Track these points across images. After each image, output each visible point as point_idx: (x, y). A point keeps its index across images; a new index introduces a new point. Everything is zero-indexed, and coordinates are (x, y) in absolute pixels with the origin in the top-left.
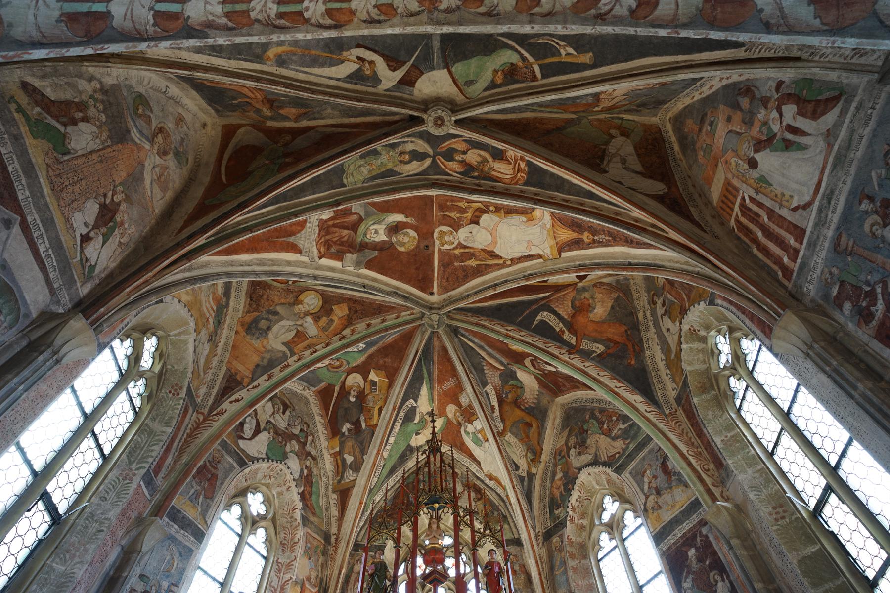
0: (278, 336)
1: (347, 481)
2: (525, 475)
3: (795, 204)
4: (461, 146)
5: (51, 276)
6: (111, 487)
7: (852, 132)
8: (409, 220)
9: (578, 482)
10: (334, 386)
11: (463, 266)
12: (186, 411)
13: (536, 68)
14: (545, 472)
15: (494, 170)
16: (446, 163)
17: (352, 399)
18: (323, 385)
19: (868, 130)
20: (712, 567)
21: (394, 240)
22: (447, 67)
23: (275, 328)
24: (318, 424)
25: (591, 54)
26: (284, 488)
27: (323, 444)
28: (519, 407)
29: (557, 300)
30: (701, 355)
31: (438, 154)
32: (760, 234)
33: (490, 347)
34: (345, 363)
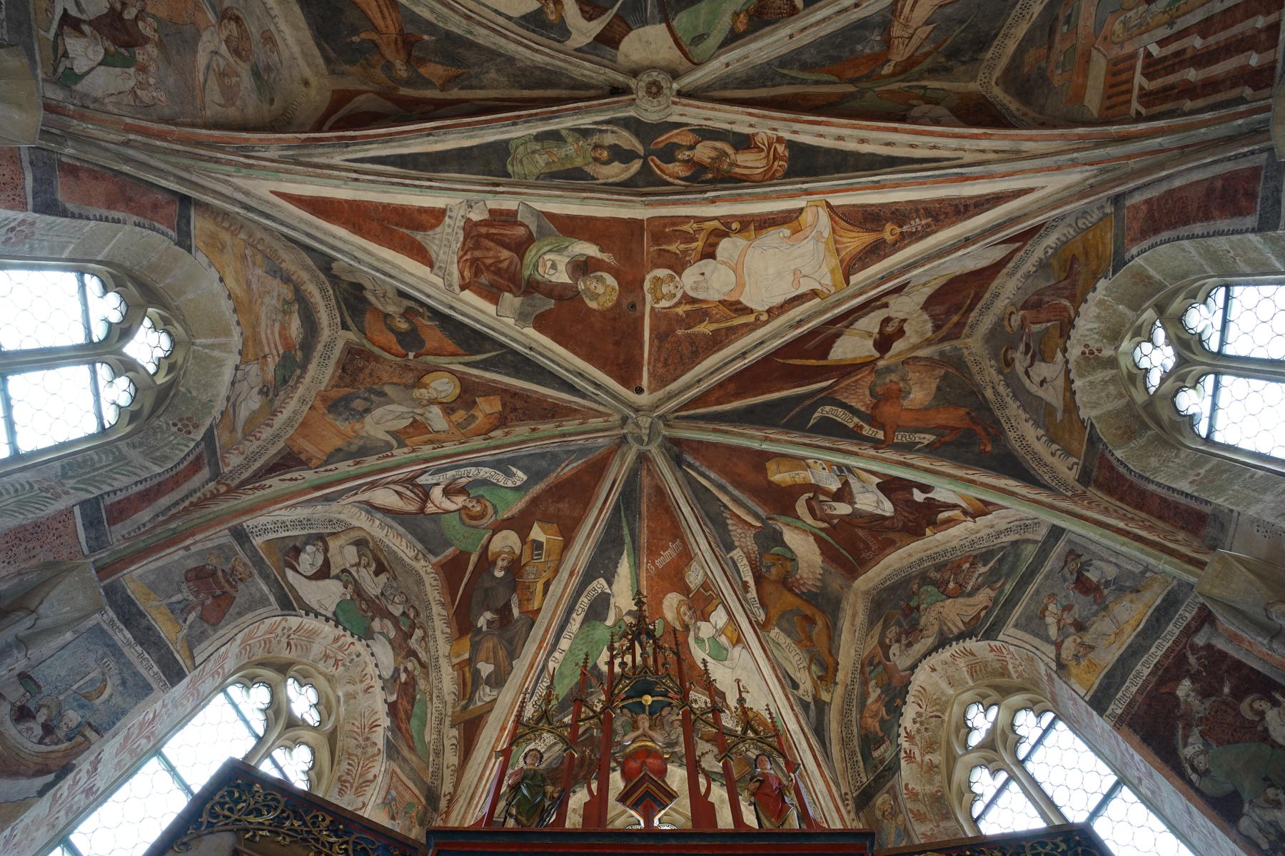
0: (381, 422)
1: (479, 704)
2: (810, 699)
4: (685, 139)
6: (12, 490)
8: (606, 257)
9: (913, 689)
10: (470, 554)
11: (690, 334)
12: (195, 466)
14: (847, 701)
15: (738, 166)
16: (664, 166)
17: (499, 574)
18: (450, 551)
20: (1238, 695)
21: (581, 286)
22: (666, 20)
23: (378, 413)
24: (436, 618)
26: (360, 687)
27: (440, 643)
28: (791, 590)
29: (846, 388)
30: (1111, 388)
32: (1192, 74)
33: (738, 485)
34: (490, 510)
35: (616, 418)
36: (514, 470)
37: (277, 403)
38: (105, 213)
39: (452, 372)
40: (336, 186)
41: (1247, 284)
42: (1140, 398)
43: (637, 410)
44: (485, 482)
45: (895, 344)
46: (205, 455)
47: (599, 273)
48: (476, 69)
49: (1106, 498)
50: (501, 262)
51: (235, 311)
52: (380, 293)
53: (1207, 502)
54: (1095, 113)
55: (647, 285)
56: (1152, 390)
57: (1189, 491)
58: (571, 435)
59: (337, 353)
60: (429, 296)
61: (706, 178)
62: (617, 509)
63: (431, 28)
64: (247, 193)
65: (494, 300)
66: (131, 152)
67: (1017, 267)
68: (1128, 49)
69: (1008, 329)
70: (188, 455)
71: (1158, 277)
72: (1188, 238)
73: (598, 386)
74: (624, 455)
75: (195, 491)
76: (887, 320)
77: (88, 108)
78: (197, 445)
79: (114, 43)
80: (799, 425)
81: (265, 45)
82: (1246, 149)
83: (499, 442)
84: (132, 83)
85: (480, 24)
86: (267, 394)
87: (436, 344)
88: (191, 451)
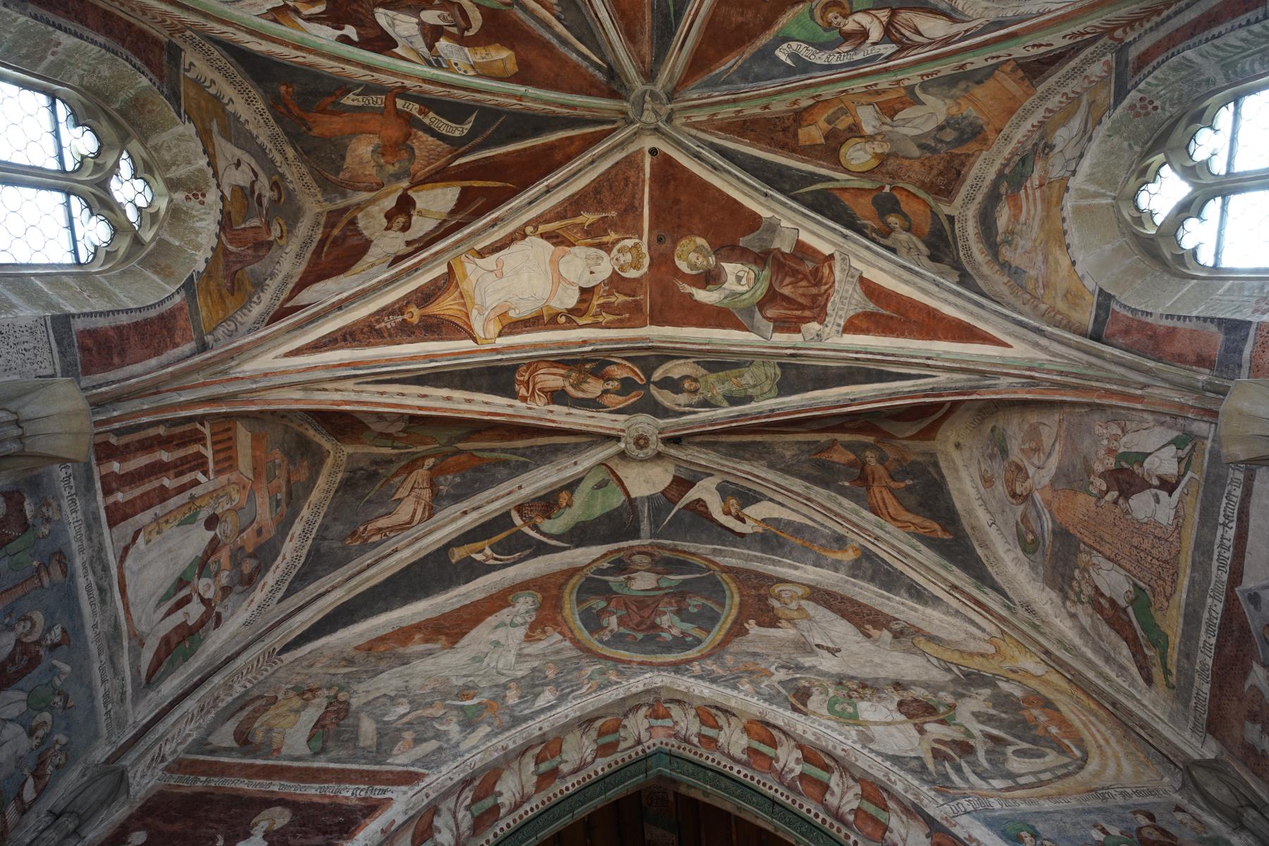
0: (929, 114)
3: (141, 540)
4: (611, 399)
5: (1238, 492)
7: (117, 672)
12: (1143, 60)
13: (518, 520)
16: (631, 375)
19: (101, 692)
21: (712, 260)
22: (631, 501)
23: (931, 126)
25: (453, 561)
29: (439, 156)
30: (167, 157)
32: (165, 456)
33: (547, 45)
34: (818, 13)
35: (678, 121)
36: (789, 62)
37: (1036, 136)
38: (1179, 324)
39: (847, 171)
40: (948, 353)
41: (60, 265)
42: (135, 145)
43: (657, 130)
44: (822, 47)
45: (394, 204)
47: (694, 272)
49: (145, 27)
50: (791, 283)
51: (1065, 233)
52: (914, 252)
53: (35, 17)
54: (239, 425)
55: (646, 261)
56: (125, 155)
57: (59, 33)
58: (727, 102)
59: (963, 192)
60: (868, 248)
61: (590, 364)
62: (679, 15)
63: (842, 491)
64: (1036, 345)
65: (800, 245)
66: (1142, 379)
67: (285, 283)
68: (223, 479)
69: (282, 222)
70: (1150, 73)
71: (148, 273)
72: (131, 310)
73: (698, 156)
74: (670, 80)
75: (1151, 29)
76: (405, 228)
77: (1169, 415)
78: (1137, 84)
79: (1133, 472)
80: (488, 114)
82: (103, 389)
83: (805, 92)
84: (1124, 439)
85: (799, 495)
86: (1046, 145)
87: (862, 200)
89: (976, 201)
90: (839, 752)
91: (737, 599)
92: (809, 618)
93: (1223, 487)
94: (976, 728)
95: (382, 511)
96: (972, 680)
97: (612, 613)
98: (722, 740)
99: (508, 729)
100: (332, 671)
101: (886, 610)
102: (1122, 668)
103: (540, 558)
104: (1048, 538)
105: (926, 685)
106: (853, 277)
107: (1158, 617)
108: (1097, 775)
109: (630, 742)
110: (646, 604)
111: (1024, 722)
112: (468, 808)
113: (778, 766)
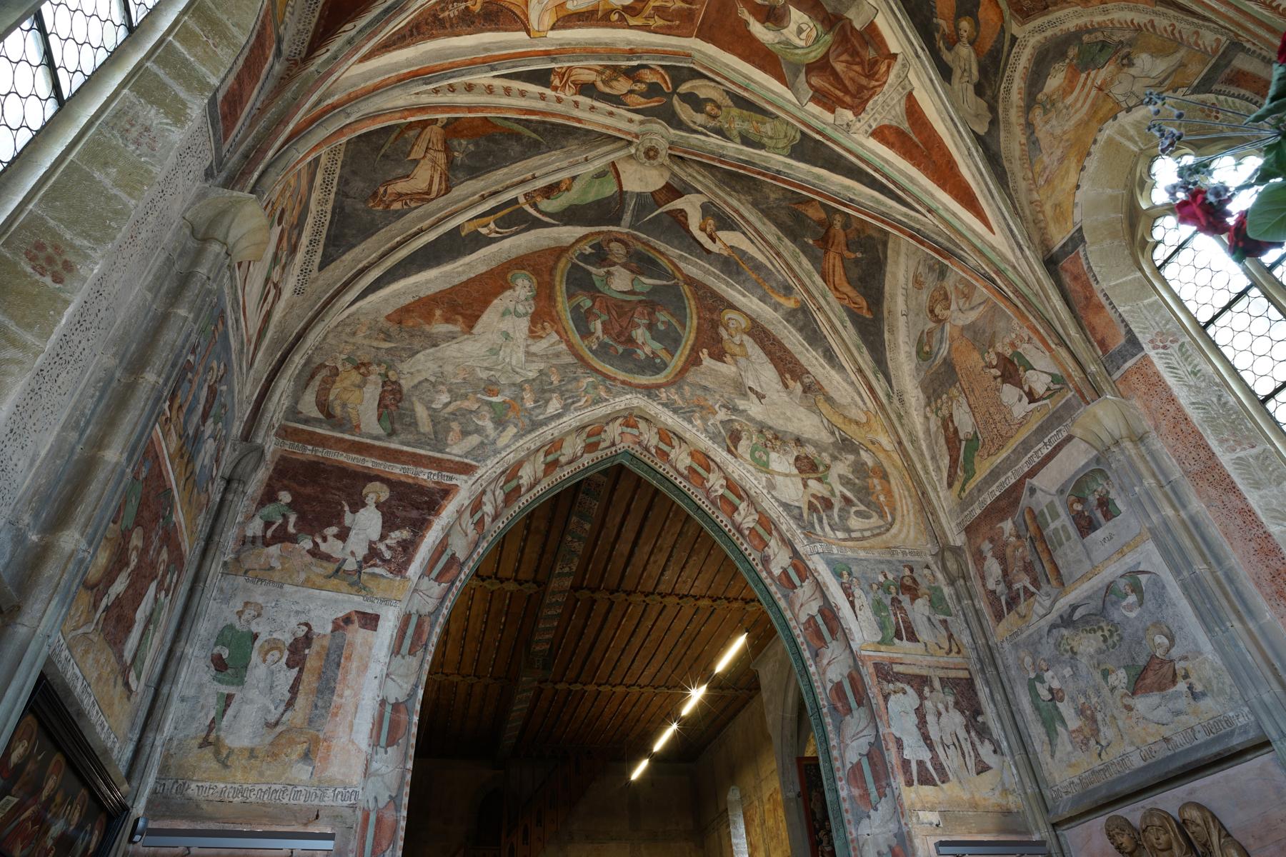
8: (745, 15)
12: (1239, 79)
22: (622, 193)
31: (666, 95)
37: (1128, 35)
38: (1108, 308)
46: (1223, 76)
48: (783, 204)
50: (847, 62)
51: (1089, 154)
60: (931, 80)
63: (805, 249)
65: (872, 27)
70: (1233, 96)
78: (1219, 93)
79: (1017, 370)
81: (923, 283)
84: (1026, 345)
86: (1127, 56)
88: (1228, 95)
89: (1044, 34)
90: (752, 492)
91: (695, 322)
92: (747, 356)
93: (1060, 424)
94: (839, 488)
95: (400, 171)
96: (846, 445)
97: (598, 317)
98: (672, 456)
99: (530, 432)
100: (375, 344)
101: (803, 361)
102: (938, 468)
103: (532, 231)
104: (939, 360)
105: (816, 445)
106: (904, 88)
107: (977, 459)
108: (895, 536)
109: (607, 443)
110: (620, 311)
111: (867, 488)
112: (502, 488)
113: (708, 485)
